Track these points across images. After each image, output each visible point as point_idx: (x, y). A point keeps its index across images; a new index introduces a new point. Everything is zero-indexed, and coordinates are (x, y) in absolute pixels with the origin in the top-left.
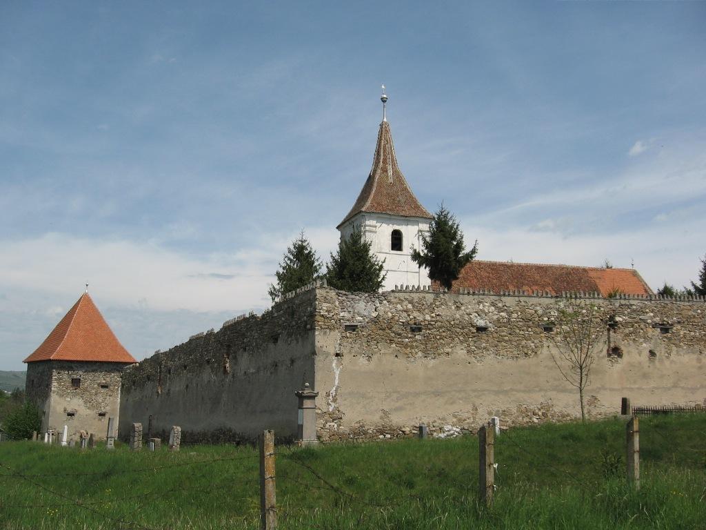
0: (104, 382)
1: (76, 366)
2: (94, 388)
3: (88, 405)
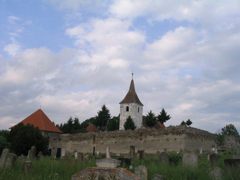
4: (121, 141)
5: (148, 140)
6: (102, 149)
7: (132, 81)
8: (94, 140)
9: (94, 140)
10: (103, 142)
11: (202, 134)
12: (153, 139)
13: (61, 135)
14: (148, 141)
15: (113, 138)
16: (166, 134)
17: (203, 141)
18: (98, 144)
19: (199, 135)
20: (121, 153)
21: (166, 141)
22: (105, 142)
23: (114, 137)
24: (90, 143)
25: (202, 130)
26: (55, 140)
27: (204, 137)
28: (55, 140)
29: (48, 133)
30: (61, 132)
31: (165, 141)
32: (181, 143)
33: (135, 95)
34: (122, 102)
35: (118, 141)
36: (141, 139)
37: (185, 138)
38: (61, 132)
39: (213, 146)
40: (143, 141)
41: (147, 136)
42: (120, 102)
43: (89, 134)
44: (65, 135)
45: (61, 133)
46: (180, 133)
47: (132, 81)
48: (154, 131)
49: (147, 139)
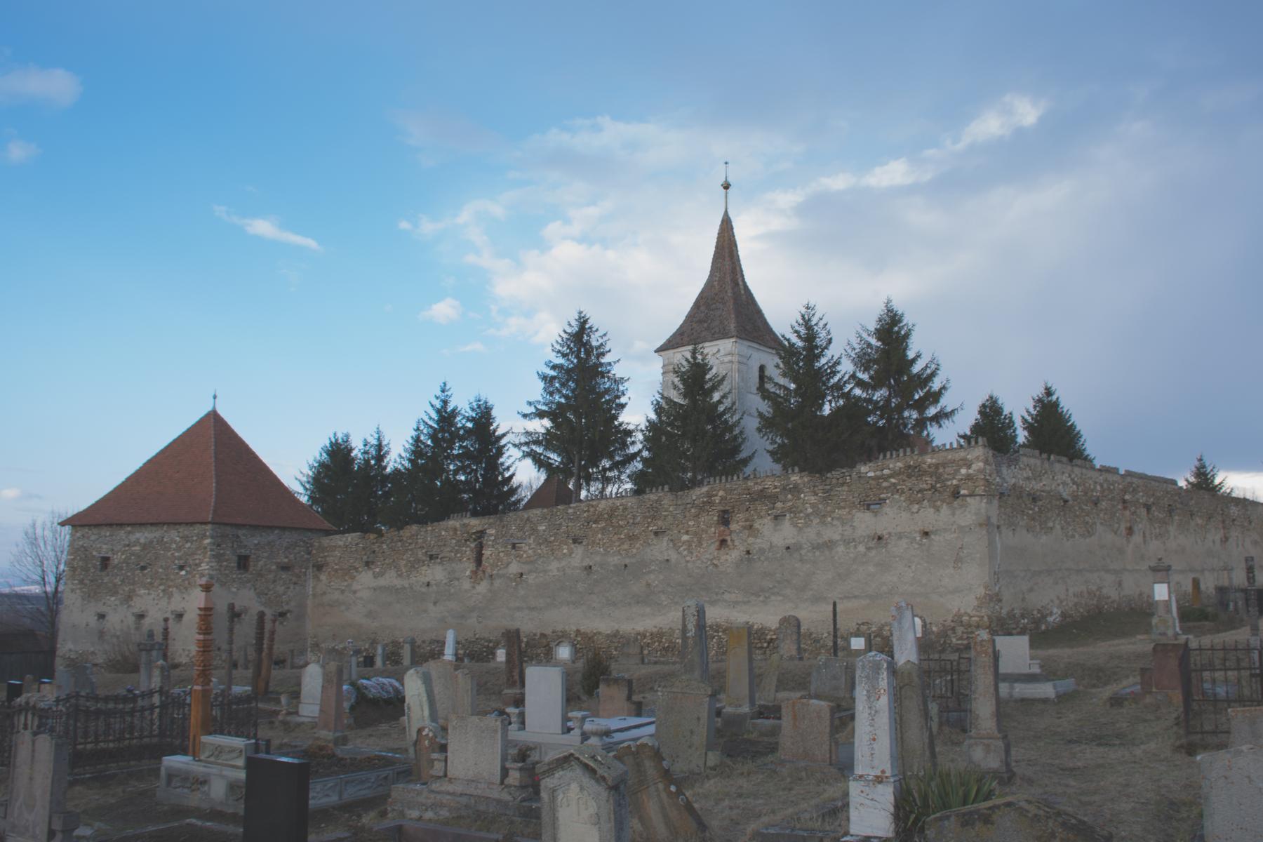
0: (286, 560)
1: (244, 535)
2: (270, 571)
3: (263, 600)
4: (615, 560)
5: (766, 546)
6: (519, 609)
7: (726, 228)
8: (479, 560)
9: (479, 560)
10: (525, 568)
11: (1127, 497)
12: (789, 542)
13: (326, 541)
14: (762, 551)
15: (575, 541)
16: (868, 507)
17: (1137, 538)
18: (497, 583)
19: (1104, 504)
20: (616, 627)
21: (869, 549)
22: (530, 572)
23: (576, 541)
24: (458, 579)
25: (1129, 474)
26: (285, 568)
27: (1143, 511)
28: (285, 568)
29: (240, 532)
30: (328, 525)
31: (861, 548)
32: (958, 560)
33: (736, 297)
34: (669, 341)
35: (598, 558)
36: (723, 542)
37: (986, 523)
38: (328, 525)
39: (804, 722)
40: (734, 555)
41: (756, 525)
42: (655, 349)
43: (455, 530)
44: (339, 540)
45: (328, 533)
46: (956, 494)
47: (726, 228)
48: (796, 489)
49: (757, 543)
